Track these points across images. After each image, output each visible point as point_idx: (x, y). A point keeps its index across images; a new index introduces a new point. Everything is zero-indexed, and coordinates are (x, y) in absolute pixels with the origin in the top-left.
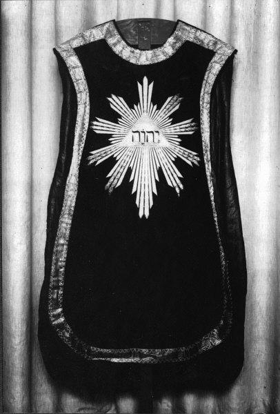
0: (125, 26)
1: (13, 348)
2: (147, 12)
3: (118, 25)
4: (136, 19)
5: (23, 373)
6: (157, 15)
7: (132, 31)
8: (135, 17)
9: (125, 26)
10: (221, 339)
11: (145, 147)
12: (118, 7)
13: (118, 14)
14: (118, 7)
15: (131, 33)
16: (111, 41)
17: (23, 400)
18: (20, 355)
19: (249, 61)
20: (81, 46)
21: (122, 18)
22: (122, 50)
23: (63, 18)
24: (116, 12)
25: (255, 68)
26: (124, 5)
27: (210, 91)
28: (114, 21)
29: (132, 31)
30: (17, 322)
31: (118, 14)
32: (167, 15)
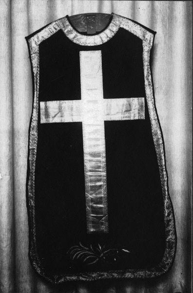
0: (76, 19)
1: (2, 249)
2: (92, 8)
3: (73, 20)
4: (85, 14)
5: (9, 267)
6: (99, 11)
7: (82, 22)
8: (85, 12)
9: (76, 19)
10: (169, 242)
11: (93, 111)
12: (72, 6)
13: (72, 11)
14: (72, 6)
15: (81, 24)
16: (135, 102)
17: (10, 287)
18: (7, 254)
19: (165, 43)
20: (151, 130)
21: (75, 13)
22: (73, 36)
23: (33, 13)
24: (71, 9)
25: (170, 49)
26: (76, 3)
27: (89, 2)
28: (67, 16)
29: (82, 22)
30: (4, 231)
31: (72, 11)
32: (107, 10)
